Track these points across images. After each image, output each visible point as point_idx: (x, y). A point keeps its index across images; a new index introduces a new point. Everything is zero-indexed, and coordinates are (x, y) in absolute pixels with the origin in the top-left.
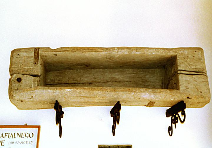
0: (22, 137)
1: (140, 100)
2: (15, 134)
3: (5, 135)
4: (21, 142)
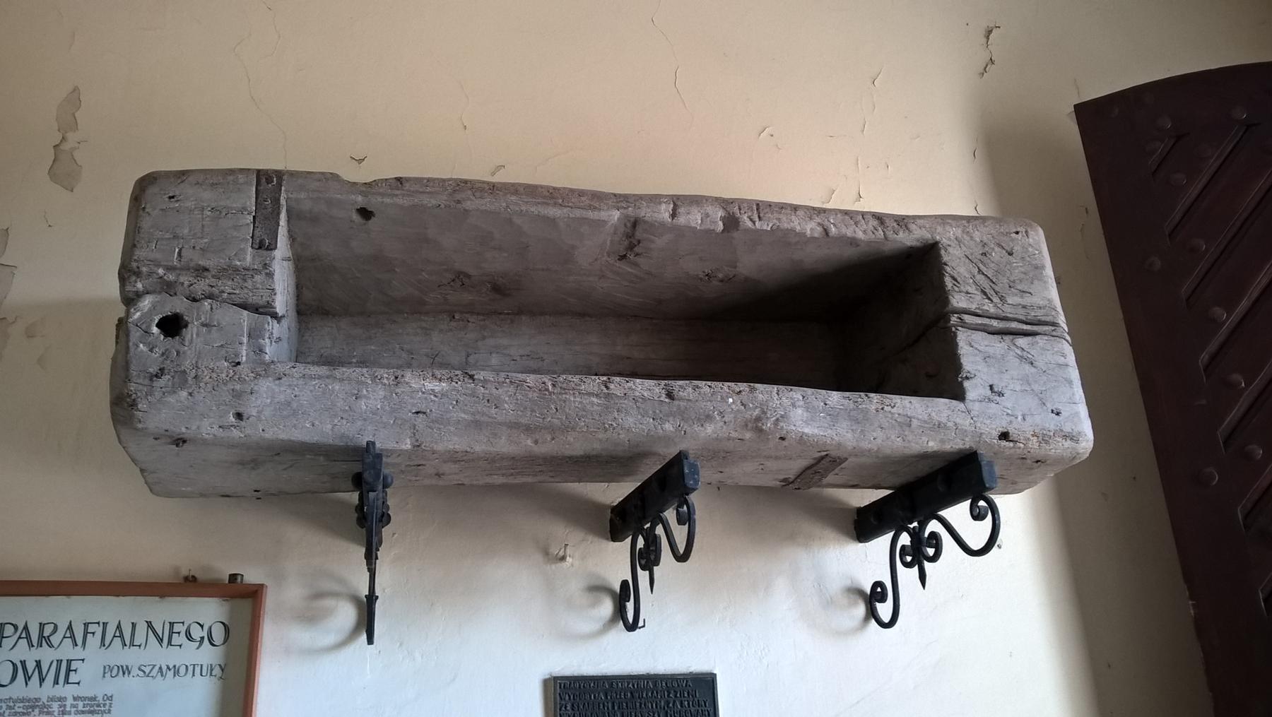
0: (170, 643)
1: (785, 443)
2: (134, 625)
3: (86, 633)
4: (164, 668)
